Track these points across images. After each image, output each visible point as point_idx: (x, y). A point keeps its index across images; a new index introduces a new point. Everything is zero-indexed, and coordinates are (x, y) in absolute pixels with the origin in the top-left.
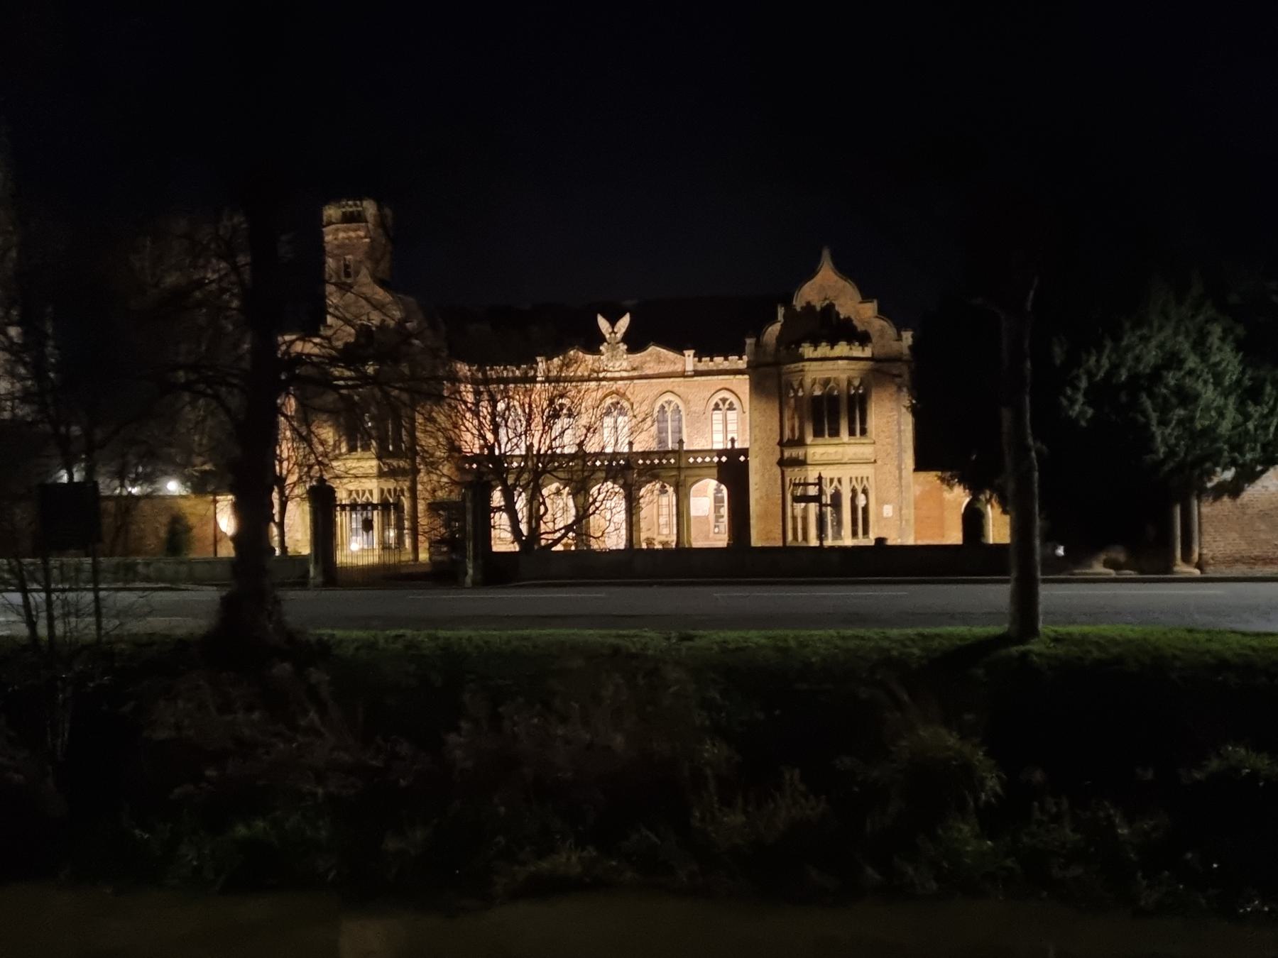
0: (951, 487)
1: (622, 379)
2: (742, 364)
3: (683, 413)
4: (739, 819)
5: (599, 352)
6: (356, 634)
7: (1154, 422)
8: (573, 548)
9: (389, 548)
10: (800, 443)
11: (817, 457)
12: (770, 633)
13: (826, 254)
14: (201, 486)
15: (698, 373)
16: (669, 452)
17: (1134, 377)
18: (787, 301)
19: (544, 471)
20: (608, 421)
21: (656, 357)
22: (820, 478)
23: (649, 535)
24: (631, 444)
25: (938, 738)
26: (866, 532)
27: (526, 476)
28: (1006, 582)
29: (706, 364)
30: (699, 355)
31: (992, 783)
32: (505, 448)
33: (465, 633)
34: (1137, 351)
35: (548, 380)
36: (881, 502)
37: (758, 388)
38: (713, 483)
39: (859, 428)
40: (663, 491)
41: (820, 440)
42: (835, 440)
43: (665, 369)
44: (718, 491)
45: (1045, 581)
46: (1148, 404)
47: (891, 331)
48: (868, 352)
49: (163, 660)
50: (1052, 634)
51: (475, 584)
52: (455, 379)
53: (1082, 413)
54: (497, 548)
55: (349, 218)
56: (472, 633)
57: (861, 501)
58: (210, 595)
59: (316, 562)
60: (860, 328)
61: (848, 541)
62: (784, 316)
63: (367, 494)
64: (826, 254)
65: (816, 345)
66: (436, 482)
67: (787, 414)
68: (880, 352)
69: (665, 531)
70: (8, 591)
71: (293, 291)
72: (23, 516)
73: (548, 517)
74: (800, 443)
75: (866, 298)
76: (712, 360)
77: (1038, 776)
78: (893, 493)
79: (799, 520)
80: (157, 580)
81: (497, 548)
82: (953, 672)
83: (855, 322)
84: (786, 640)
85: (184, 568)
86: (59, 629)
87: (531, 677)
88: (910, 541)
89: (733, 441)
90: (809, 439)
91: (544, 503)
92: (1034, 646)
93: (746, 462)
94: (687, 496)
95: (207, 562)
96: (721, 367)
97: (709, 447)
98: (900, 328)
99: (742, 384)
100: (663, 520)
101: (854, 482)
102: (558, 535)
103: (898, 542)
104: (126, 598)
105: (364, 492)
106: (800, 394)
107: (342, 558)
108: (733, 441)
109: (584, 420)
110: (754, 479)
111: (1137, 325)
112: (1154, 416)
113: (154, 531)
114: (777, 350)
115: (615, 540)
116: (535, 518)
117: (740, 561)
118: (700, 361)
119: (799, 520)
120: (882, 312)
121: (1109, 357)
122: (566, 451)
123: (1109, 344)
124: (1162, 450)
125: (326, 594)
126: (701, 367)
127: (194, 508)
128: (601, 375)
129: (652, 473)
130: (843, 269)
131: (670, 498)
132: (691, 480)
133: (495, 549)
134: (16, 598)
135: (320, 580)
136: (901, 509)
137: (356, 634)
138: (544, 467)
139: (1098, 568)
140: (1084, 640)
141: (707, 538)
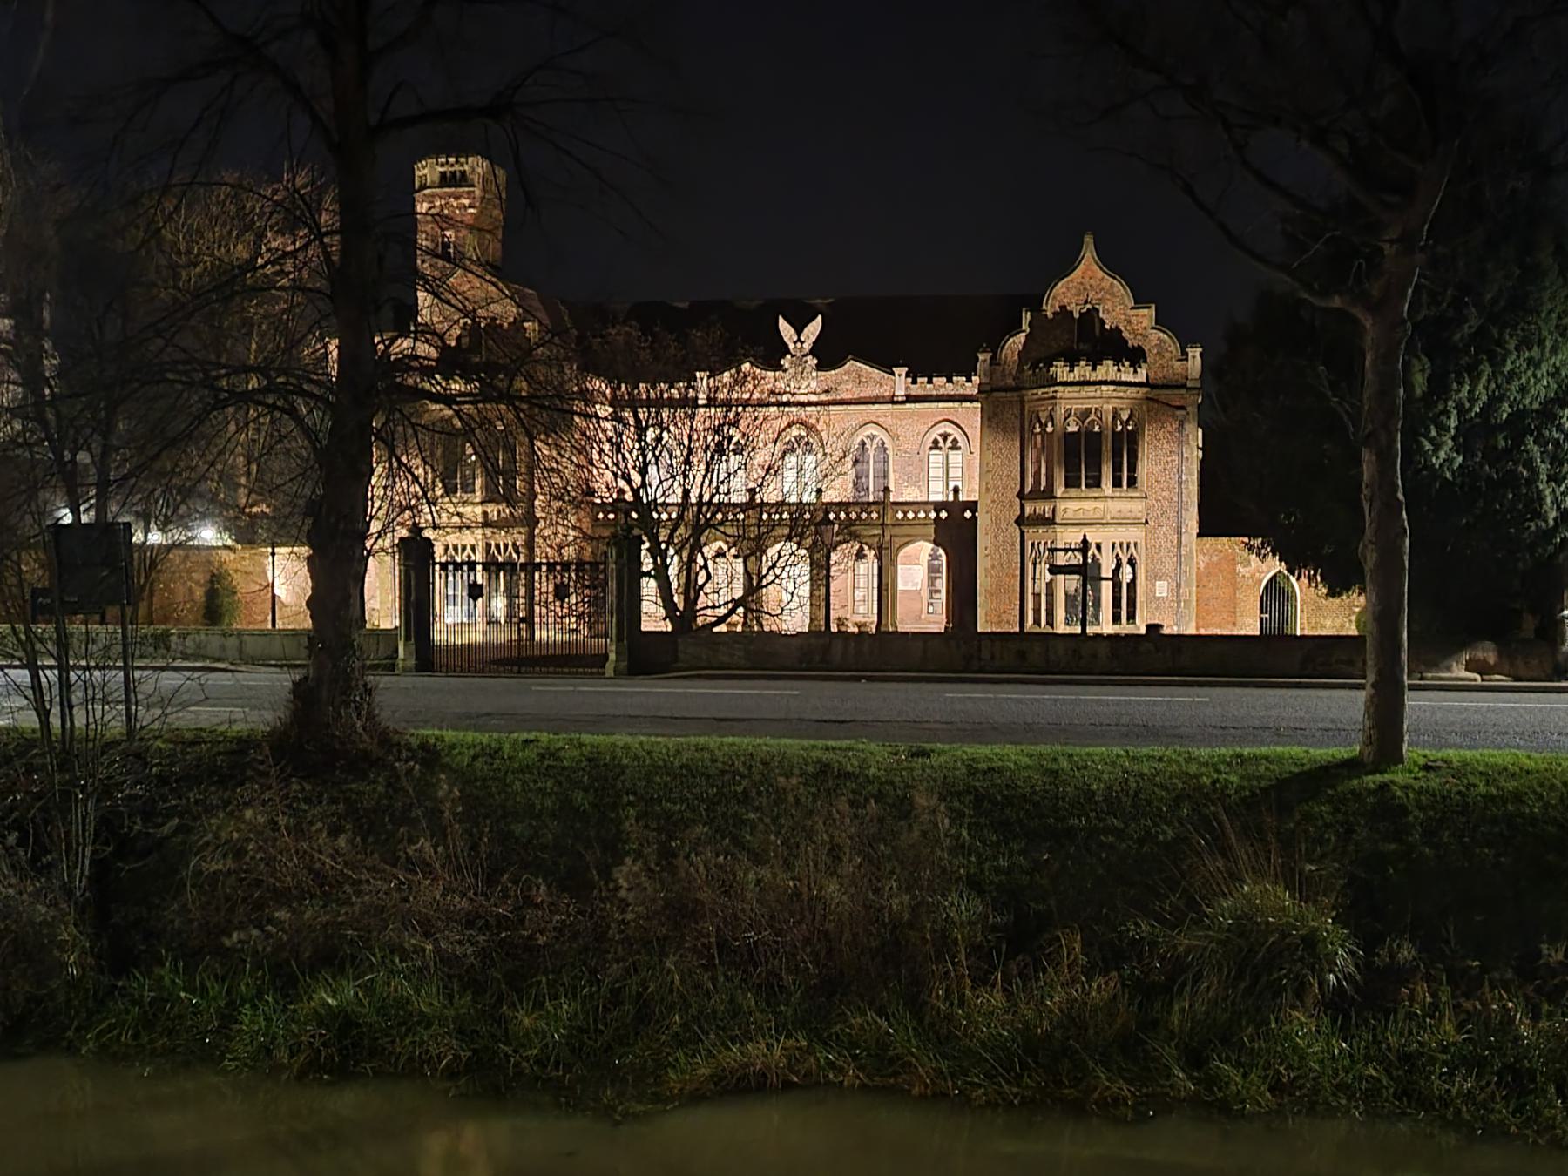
0: (1263, 558)
1: (810, 404)
2: (971, 388)
3: (889, 452)
4: (997, 1000)
5: (779, 367)
6: (470, 736)
7: (1544, 477)
8: (739, 628)
9: (497, 622)
10: (1049, 494)
11: (1070, 514)
12: (1032, 749)
13: (1089, 240)
14: (247, 534)
15: (910, 399)
16: (869, 504)
17: (1519, 415)
18: (1036, 305)
19: (708, 524)
20: (791, 460)
21: (856, 376)
22: (1085, 541)
23: (841, 614)
24: (819, 491)
25: (1266, 897)
26: (1131, 617)
27: (681, 530)
28: (1362, 687)
29: (922, 387)
30: (913, 375)
31: (1342, 959)
32: (654, 493)
33: (621, 739)
34: (1523, 380)
35: (711, 402)
36: (1154, 577)
37: (991, 420)
38: (926, 547)
39: (1127, 478)
40: (860, 555)
41: (1073, 492)
42: (1095, 493)
43: (867, 392)
44: (934, 557)
45: (1412, 688)
46: (1536, 451)
47: (1173, 348)
48: (1141, 376)
49: (223, 765)
50: (1422, 761)
51: (618, 673)
52: (588, 398)
53: (1449, 460)
54: (647, 626)
55: (446, 180)
56: (629, 739)
57: (1126, 574)
58: (283, 681)
59: (407, 638)
60: (1132, 342)
61: (1107, 627)
62: (1030, 325)
63: (468, 550)
64: (1089, 240)
65: (1072, 363)
66: (560, 536)
67: (1030, 455)
68: (1158, 376)
69: (862, 610)
70: (9, 667)
71: (373, 273)
72: (33, 568)
73: (708, 588)
74: (1049, 494)
75: (1140, 301)
76: (930, 382)
77: (1406, 953)
78: (1169, 564)
79: (1043, 598)
80: (196, 657)
81: (647, 626)
82: (1285, 808)
83: (1126, 335)
84: (1055, 760)
85: (232, 642)
86: (80, 721)
87: (726, 799)
88: (1192, 631)
89: (956, 490)
90: (1060, 491)
91: (705, 567)
92: (1398, 776)
93: (974, 518)
94: (894, 563)
95: (263, 634)
96: (942, 391)
97: (924, 499)
98: (1184, 343)
99: (971, 415)
100: (859, 595)
101: (1118, 549)
102: (723, 611)
103: (1175, 631)
104: (169, 680)
105: (464, 548)
106: (1049, 429)
107: (439, 636)
108: (956, 490)
109: (762, 457)
110: (983, 541)
111: (1526, 343)
112: (1543, 468)
113: (189, 590)
114: (1020, 370)
115: (796, 620)
116: (692, 589)
117: (962, 652)
118: (914, 382)
119: (1043, 598)
120: (1161, 322)
121: (1486, 388)
122: (735, 499)
123: (1487, 369)
124: (1553, 514)
125: (425, 680)
126: (916, 390)
127: (236, 560)
128: (785, 398)
129: (850, 531)
130: (1110, 262)
131: (868, 568)
132: (898, 541)
133: (643, 628)
134: (23, 676)
135: (412, 662)
136: (1179, 586)
137: (470, 736)
138: (721, 523)
139: (1459, 672)
140: (1461, 771)
141: (918, 619)
